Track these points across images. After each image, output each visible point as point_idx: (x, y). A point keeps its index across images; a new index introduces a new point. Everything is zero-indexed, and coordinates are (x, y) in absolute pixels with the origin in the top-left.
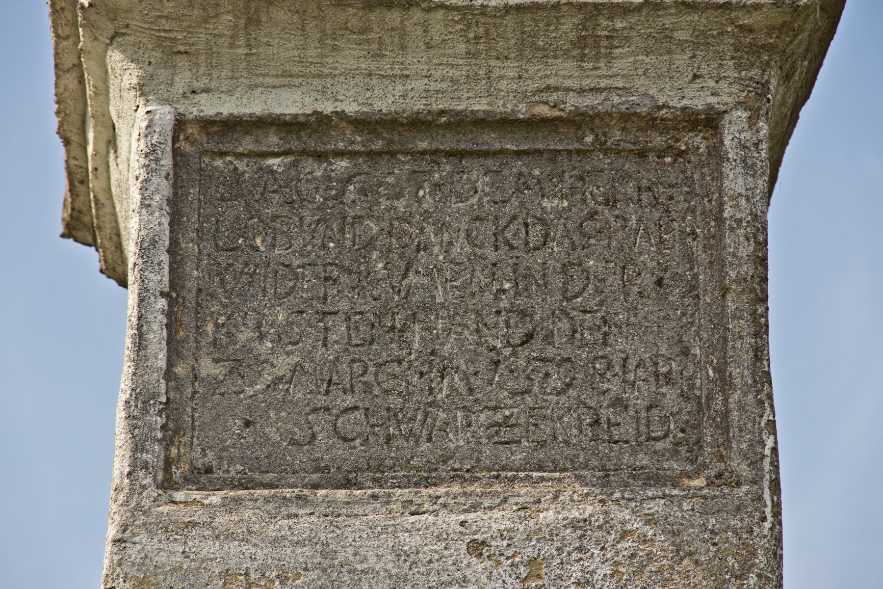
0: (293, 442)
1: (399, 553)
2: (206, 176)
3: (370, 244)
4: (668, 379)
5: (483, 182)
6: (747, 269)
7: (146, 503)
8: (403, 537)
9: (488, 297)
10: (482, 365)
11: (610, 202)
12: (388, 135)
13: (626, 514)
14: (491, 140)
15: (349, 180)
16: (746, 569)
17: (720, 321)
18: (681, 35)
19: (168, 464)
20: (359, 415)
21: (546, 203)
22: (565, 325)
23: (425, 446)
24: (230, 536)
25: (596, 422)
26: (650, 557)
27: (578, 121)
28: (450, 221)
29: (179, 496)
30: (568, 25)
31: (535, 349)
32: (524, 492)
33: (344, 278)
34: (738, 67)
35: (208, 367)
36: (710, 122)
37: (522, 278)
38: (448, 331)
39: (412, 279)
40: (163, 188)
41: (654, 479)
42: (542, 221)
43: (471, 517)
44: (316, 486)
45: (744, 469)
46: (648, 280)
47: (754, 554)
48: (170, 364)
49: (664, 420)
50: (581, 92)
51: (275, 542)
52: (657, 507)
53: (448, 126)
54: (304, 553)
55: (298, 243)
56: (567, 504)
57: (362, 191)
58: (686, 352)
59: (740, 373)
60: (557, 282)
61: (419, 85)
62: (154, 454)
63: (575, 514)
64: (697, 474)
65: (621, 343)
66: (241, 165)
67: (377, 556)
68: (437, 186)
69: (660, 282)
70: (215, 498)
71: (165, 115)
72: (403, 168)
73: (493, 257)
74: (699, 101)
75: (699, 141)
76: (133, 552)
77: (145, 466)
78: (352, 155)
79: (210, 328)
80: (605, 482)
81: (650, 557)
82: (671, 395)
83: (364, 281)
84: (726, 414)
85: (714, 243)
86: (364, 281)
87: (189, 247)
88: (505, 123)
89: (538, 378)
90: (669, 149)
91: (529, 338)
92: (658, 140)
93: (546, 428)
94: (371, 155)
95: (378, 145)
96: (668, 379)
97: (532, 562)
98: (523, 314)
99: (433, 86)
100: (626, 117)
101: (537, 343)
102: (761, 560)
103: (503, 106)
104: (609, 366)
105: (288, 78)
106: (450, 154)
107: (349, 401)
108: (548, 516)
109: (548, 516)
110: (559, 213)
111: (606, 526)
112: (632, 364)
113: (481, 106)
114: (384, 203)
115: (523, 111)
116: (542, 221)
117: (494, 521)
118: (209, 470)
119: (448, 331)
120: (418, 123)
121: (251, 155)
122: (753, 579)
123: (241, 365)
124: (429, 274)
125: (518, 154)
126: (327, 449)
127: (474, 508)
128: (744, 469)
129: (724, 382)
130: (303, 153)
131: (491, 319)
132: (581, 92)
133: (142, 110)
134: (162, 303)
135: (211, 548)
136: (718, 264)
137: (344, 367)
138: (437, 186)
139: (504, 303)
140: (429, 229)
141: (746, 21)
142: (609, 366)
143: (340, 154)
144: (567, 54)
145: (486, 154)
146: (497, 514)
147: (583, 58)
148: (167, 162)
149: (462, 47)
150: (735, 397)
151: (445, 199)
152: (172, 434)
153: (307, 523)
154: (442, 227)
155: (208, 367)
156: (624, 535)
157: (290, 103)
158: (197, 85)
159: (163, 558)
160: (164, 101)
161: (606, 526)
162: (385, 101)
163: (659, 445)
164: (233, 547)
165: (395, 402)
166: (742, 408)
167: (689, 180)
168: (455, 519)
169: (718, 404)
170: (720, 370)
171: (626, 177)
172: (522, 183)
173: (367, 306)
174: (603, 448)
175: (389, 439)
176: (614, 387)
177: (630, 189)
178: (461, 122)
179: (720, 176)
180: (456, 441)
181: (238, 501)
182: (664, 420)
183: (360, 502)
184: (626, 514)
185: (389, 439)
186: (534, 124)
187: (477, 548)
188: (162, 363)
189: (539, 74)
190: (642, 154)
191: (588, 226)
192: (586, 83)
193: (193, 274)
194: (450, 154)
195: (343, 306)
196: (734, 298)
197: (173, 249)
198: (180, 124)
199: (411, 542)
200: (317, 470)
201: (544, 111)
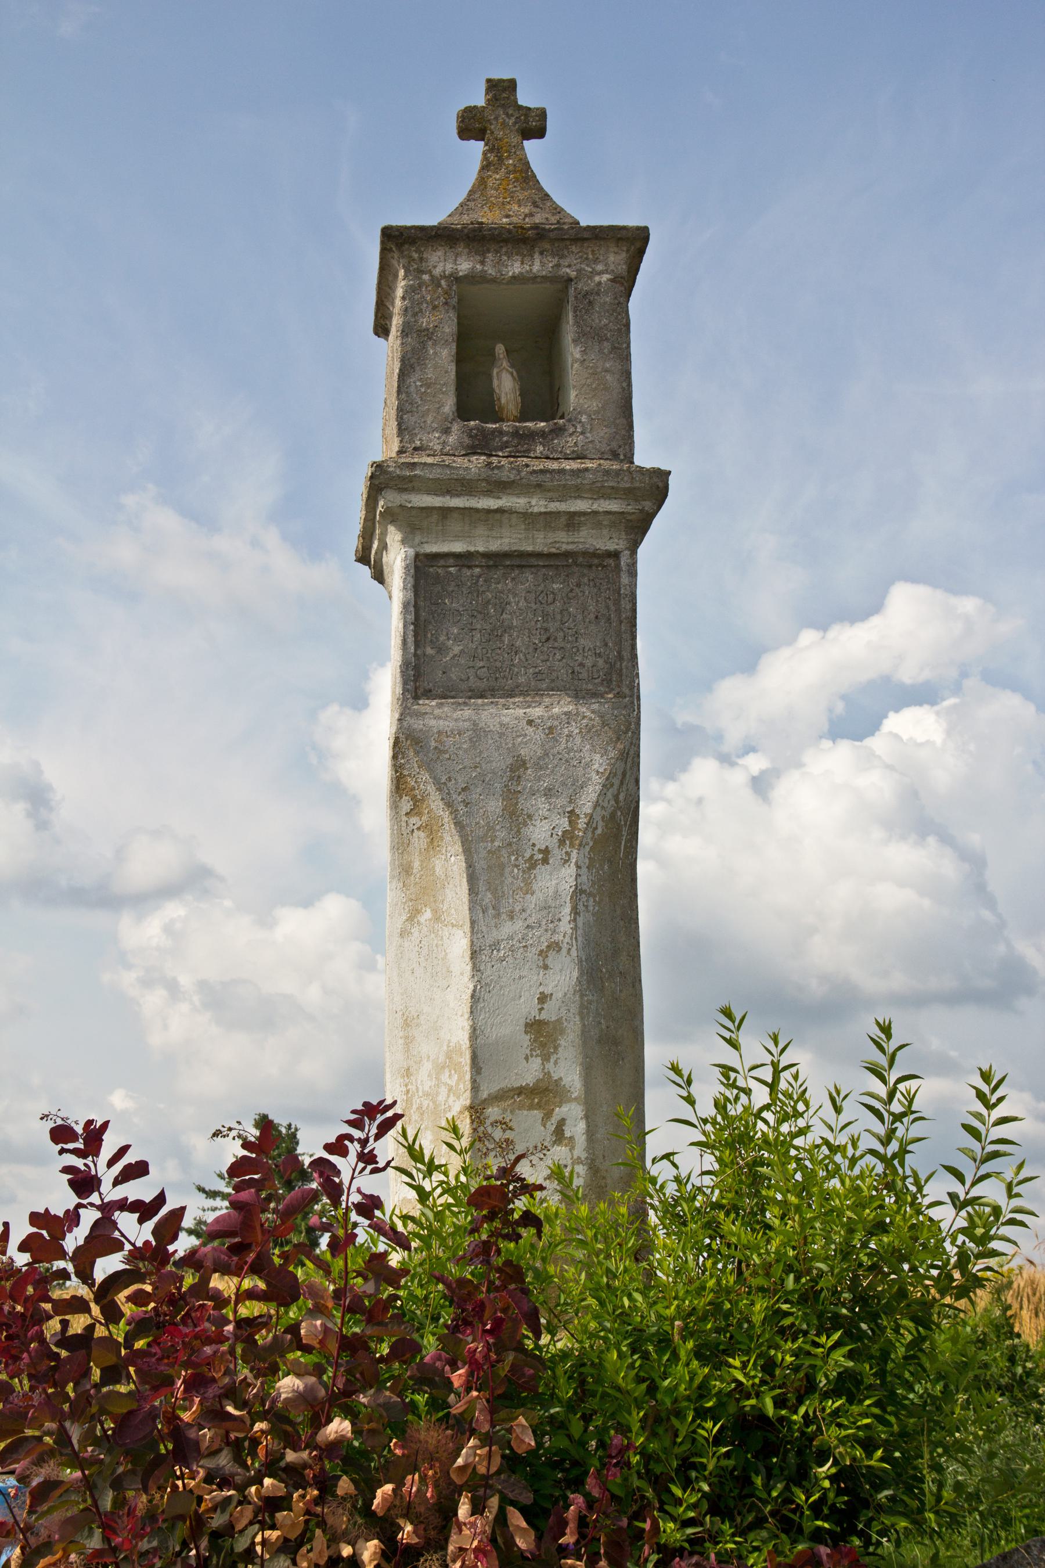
0: (461, 680)
1: (501, 725)
3: (488, 602)
4: (600, 655)
5: (530, 577)
6: (629, 614)
7: (409, 705)
8: (503, 718)
9: (533, 623)
10: (531, 650)
11: (578, 585)
12: (495, 560)
13: (584, 710)
14: (534, 561)
15: (480, 576)
16: (628, 729)
17: (619, 634)
18: (605, 523)
19: (416, 688)
20: (485, 669)
21: (555, 586)
22: (561, 634)
23: (510, 682)
24: (440, 718)
25: (573, 672)
26: (593, 726)
27: (567, 554)
28: (519, 591)
29: (421, 702)
30: (563, 520)
31: (550, 644)
32: (547, 700)
33: (479, 616)
34: (626, 534)
35: (429, 651)
37: (545, 615)
38: (518, 637)
39: (504, 616)
40: (411, 580)
41: (595, 695)
42: (553, 593)
43: (528, 710)
44: (470, 698)
45: (627, 691)
46: (592, 616)
47: (630, 724)
48: (416, 650)
49: (598, 671)
50: (568, 543)
51: (456, 720)
52: (595, 707)
53: (517, 556)
54: (467, 724)
55: (461, 602)
56: (562, 706)
57: (485, 581)
58: (606, 645)
59: (626, 654)
60: (558, 617)
61: (507, 540)
63: (566, 709)
64: (610, 692)
65: (582, 641)
66: (440, 571)
67: (493, 725)
68: (513, 579)
69: (597, 617)
70: (434, 703)
71: (411, 552)
72: (499, 573)
73: (534, 607)
74: (611, 546)
76: (405, 724)
77: (408, 690)
78: (481, 567)
79: (429, 635)
80: (576, 696)
81: (593, 726)
82: (601, 662)
83: (486, 616)
84: (621, 670)
85: (617, 603)
86: (486, 616)
88: (539, 555)
89: (551, 655)
90: (600, 565)
91: (548, 639)
92: (596, 561)
93: (555, 674)
94: (488, 567)
95: (491, 563)
96: (600, 655)
97: (550, 728)
98: (546, 630)
99: (512, 541)
100: (585, 553)
101: (551, 641)
102: (633, 726)
104: (578, 650)
105: (457, 537)
106: (518, 566)
107: (481, 664)
108: (556, 710)
109: (556, 710)
110: (560, 590)
111: (577, 714)
112: (586, 649)
113: (530, 548)
114: (493, 586)
115: (546, 550)
116: (553, 593)
117: (537, 712)
118: (430, 691)
119: (518, 637)
121: (443, 566)
122: (630, 734)
123: (441, 650)
124: (511, 614)
125: (544, 566)
126: (473, 683)
127: (529, 707)
128: (627, 691)
129: (620, 657)
130: (463, 566)
131: (534, 632)
132: (568, 543)
133: (403, 550)
134: (412, 627)
135: (433, 722)
136: (618, 611)
137: (479, 651)
138: (513, 579)
139: (539, 626)
140: (511, 596)
141: (629, 518)
142: (578, 650)
143: (477, 566)
144: (562, 529)
145: (531, 566)
146: (537, 709)
147: (568, 531)
148: (412, 571)
149: (523, 527)
150: (624, 664)
151: (516, 584)
152: (417, 677)
153: (467, 713)
154: (515, 595)
155: (429, 651)
156: (584, 717)
157: (458, 547)
158: (424, 540)
159: (416, 726)
160: (411, 547)
161: (577, 714)
162: (494, 546)
163: (596, 681)
164: (441, 722)
165: (498, 664)
166: (627, 668)
167: (607, 577)
168: (522, 711)
169: (618, 665)
170: (619, 653)
171: (584, 575)
173: (488, 627)
174: (576, 682)
175: (496, 679)
176: (579, 658)
177: (586, 580)
178: (522, 555)
179: (619, 577)
180: (522, 680)
181: (442, 704)
182: (598, 671)
183: (487, 704)
184: (584, 710)
185: (496, 679)
186: (550, 555)
187: (530, 722)
188: (412, 651)
189: (552, 537)
190: (590, 566)
191: (570, 595)
192: (570, 540)
194: (518, 566)
195: (479, 626)
197: (415, 606)
198: (417, 555)
199: (505, 720)
200: (470, 691)
201: (553, 550)
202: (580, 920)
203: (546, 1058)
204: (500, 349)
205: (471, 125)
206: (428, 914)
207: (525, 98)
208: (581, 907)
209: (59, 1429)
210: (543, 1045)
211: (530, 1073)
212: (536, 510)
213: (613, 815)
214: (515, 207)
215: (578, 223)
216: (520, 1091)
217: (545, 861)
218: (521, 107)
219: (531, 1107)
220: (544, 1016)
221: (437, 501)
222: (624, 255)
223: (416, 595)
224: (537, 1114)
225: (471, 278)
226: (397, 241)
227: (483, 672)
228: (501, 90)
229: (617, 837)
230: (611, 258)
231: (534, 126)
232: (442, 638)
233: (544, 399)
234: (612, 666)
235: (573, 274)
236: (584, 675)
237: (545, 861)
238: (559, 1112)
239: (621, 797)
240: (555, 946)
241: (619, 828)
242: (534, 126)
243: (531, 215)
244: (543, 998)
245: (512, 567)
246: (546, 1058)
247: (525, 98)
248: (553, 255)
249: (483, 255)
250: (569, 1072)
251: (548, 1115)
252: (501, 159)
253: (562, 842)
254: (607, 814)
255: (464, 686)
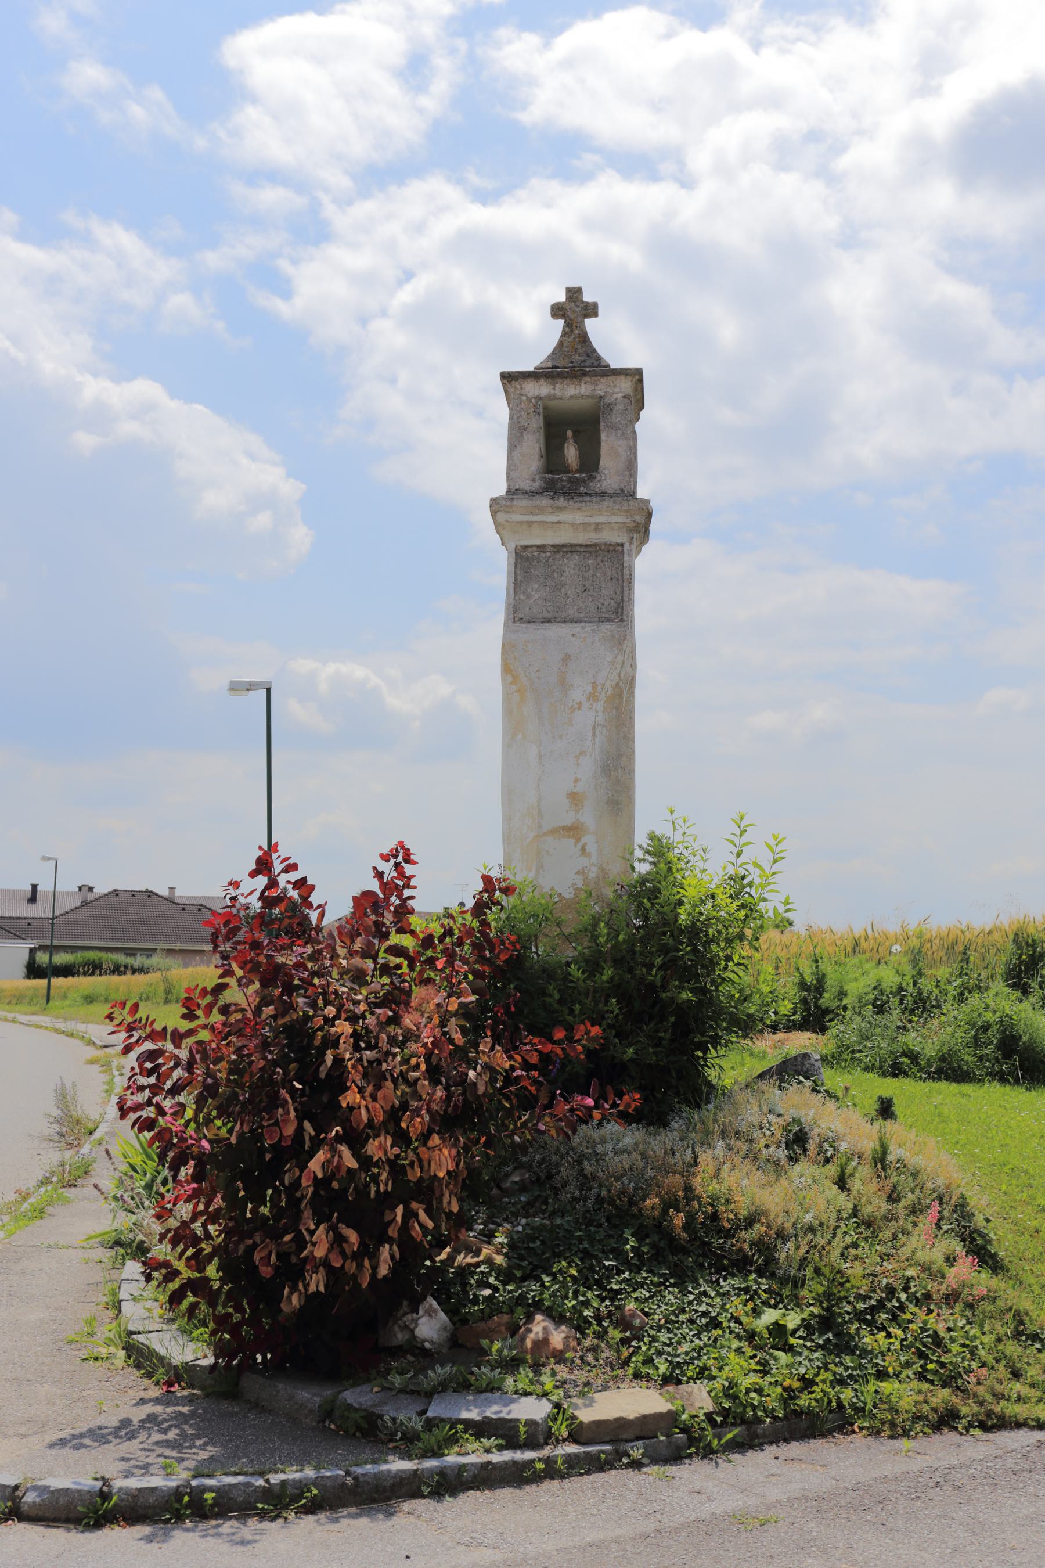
2: (522, 557)
12: (558, 548)
14: (578, 548)
27: (595, 545)
28: (570, 565)
30: (593, 527)
35: (522, 597)
36: (622, 545)
37: (584, 577)
62: (512, 616)
65: (603, 591)
72: (561, 554)
75: (620, 548)
82: (613, 603)
85: (622, 570)
87: (518, 572)
88: (581, 545)
103: (580, 542)
120: (564, 546)
123: (529, 597)
129: (622, 600)
152: (515, 611)
155: (522, 597)
172: (584, 558)
176: (601, 600)
178: (572, 545)
186: (586, 546)
193: (519, 578)
196: (623, 583)
202: (597, 740)
203: (577, 812)
204: (569, 433)
205: (558, 311)
206: (520, 736)
207: (587, 297)
208: (597, 733)
209: (550, 1034)
210: (577, 805)
211: (568, 820)
212: (578, 522)
213: (617, 684)
214: (577, 357)
215: (608, 366)
216: (563, 828)
217: (579, 709)
218: (583, 302)
219: (569, 837)
220: (576, 790)
221: (526, 518)
222: (630, 384)
223: (516, 567)
224: (573, 841)
225: (550, 397)
226: (508, 378)
227: (550, 609)
228: (574, 294)
229: (620, 695)
230: (623, 385)
231: (591, 310)
232: (529, 590)
233: (590, 463)
234: (618, 604)
235: (602, 394)
236: (604, 609)
237: (579, 709)
238: (583, 840)
239: (622, 675)
240: (582, 753)
241: (621, 691)
242: (591, 310)
243: (584, 361)
244: (576, 781)
245: (567, 552)
246: (577, 812)
247: (587, 297)
248: (592, 384)
249: (554, 384)
250: (587, 817)
251: (578, 840)
252: (572, 330)
253: (589, 699)
254: (614, 684)
255: (540, 616)
